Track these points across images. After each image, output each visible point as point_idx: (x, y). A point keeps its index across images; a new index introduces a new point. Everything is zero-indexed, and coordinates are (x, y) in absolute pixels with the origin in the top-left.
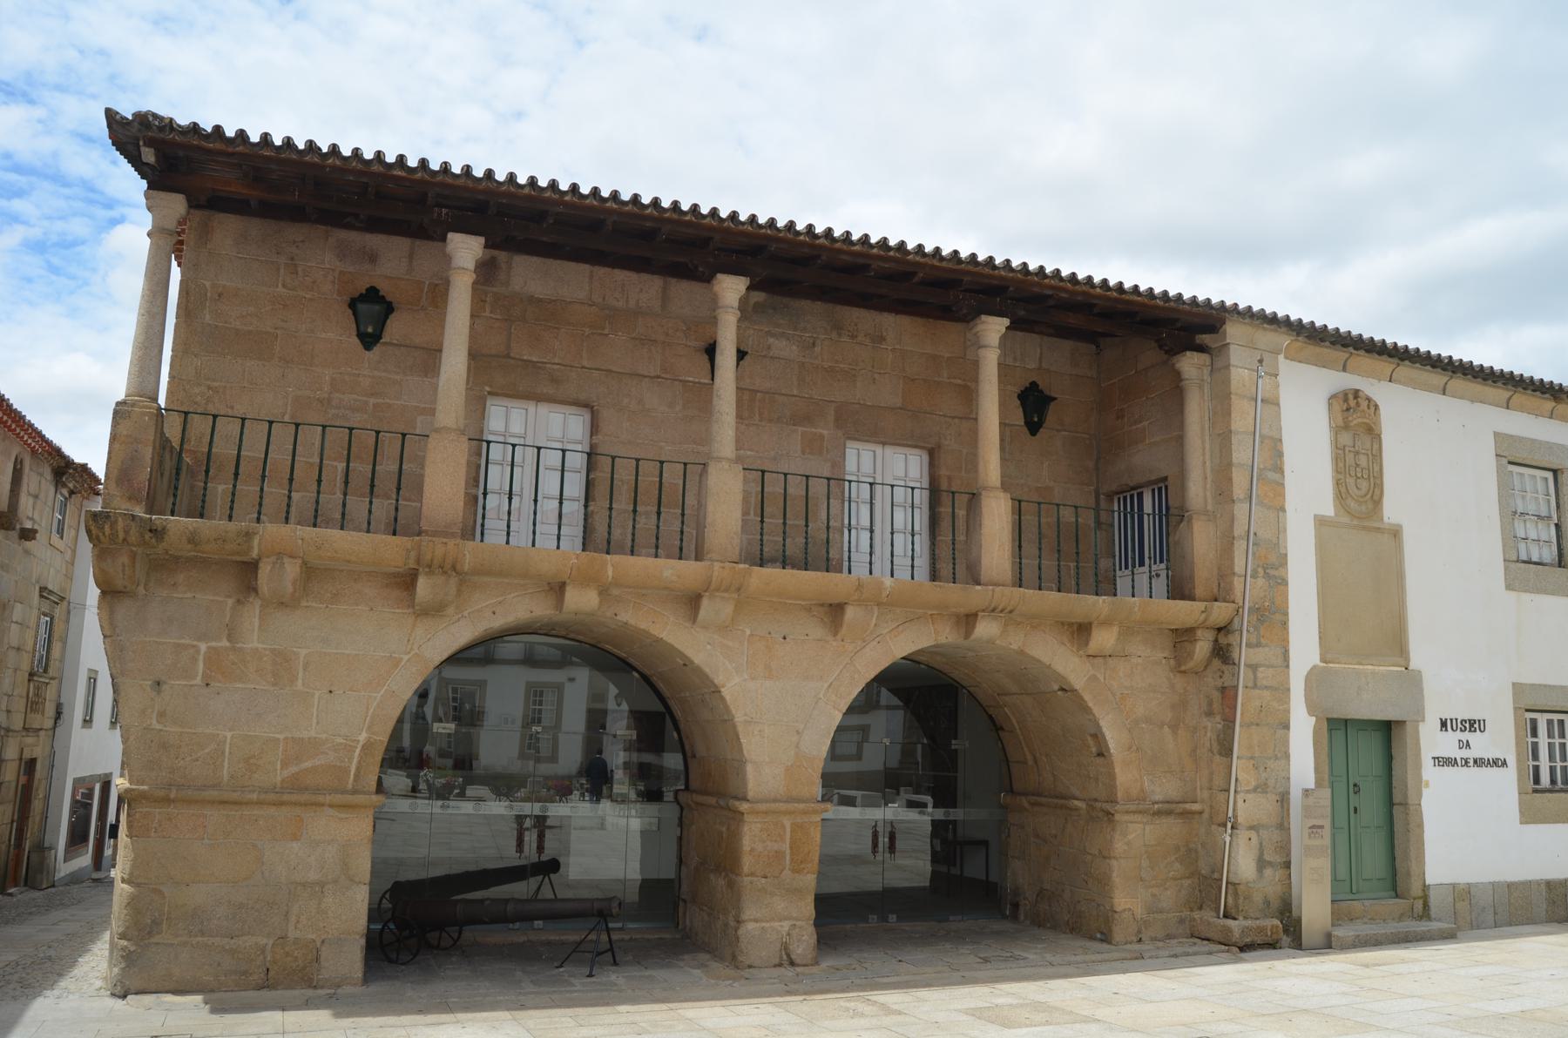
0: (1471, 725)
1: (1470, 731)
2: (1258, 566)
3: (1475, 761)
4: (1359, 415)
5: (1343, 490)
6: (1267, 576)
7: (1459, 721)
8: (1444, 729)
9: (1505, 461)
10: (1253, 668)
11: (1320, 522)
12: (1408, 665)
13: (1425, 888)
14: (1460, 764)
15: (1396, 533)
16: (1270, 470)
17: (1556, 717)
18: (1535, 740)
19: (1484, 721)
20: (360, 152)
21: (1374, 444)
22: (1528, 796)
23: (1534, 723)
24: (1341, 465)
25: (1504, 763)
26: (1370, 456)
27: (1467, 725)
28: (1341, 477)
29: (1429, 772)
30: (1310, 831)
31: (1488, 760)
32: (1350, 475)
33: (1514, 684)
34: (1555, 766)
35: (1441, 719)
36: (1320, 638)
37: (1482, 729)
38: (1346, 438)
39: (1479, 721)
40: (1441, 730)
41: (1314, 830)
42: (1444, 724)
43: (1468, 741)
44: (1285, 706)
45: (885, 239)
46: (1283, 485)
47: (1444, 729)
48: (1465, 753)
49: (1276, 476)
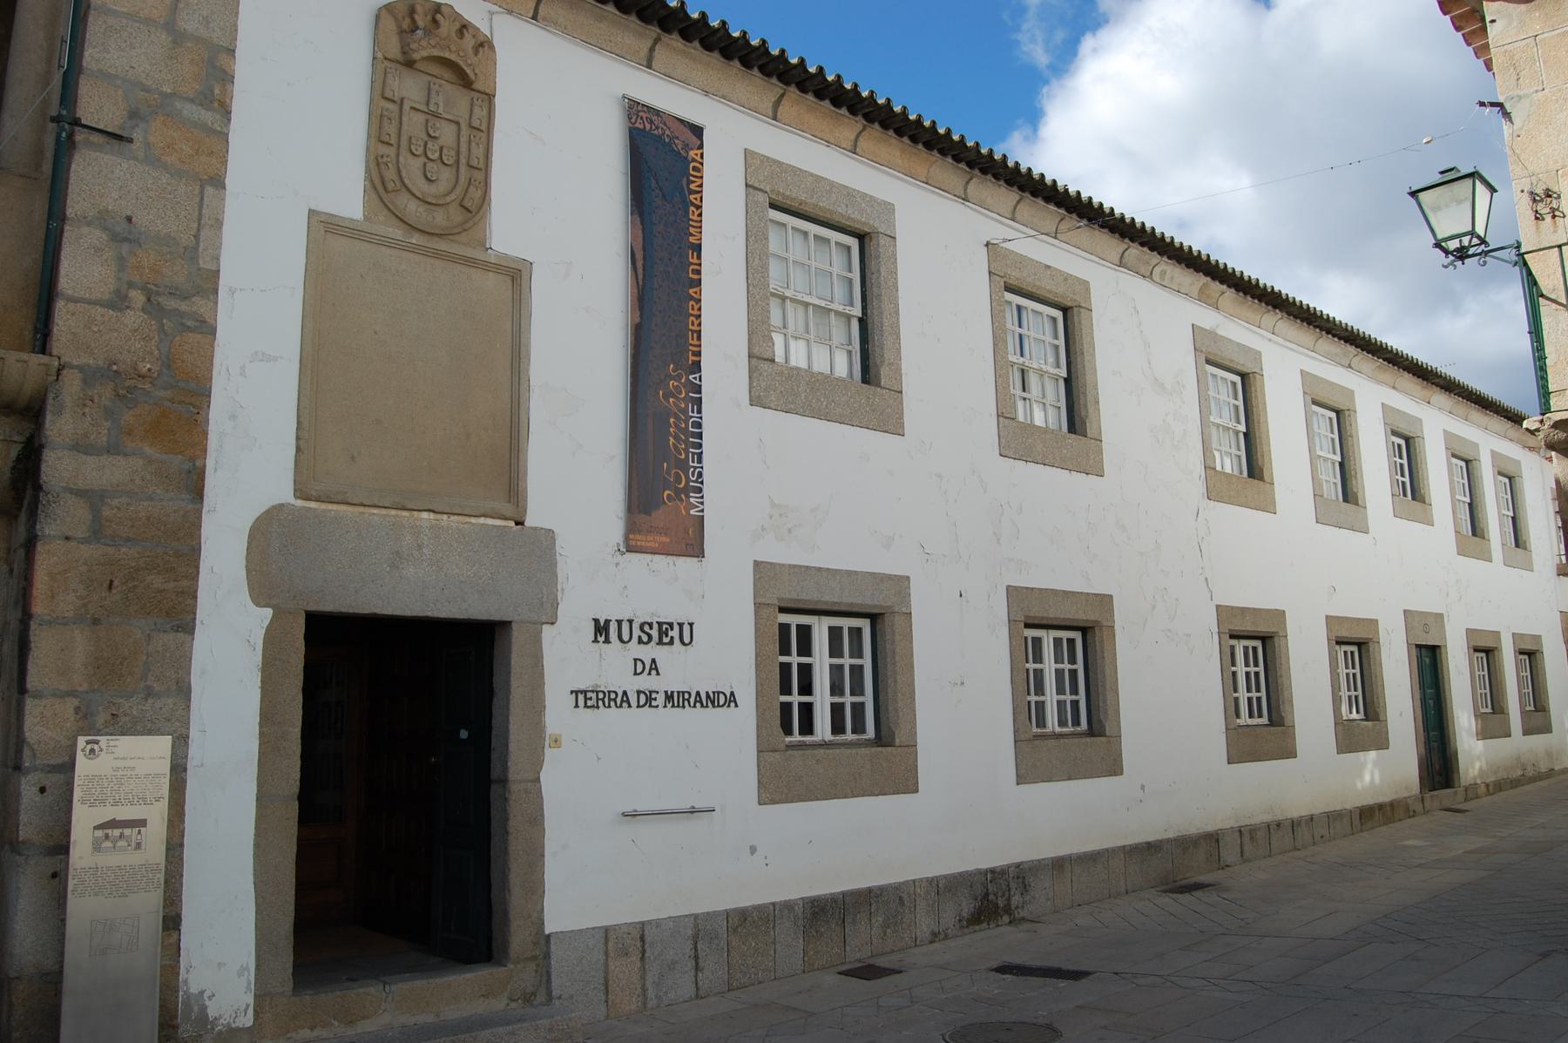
0: (663, 633)
1: (660, 642)
2: (131, 285)
3: (669, 697)
4: (433, 42)
5: (390, 174)
6: (152, 306)
7: (636, 626)
8: (601, 639)
9: (763, 199)
10: (94, 498)
11: (324, 227)
13: (545, 940)
14: (634, 702)
15: (516, 275)
16: (192, 101)
17: (846, 623)
18: (836, 661)
19: (691, 625)
21: (477, 110)
22: (777, 755)
23: (1037, 642)
24: (392, 129)
25: (732, 700)
26: (465, 131)
27: (655, 633)
28: (385, 150)
29: (558, 713)
30: (99, 833)
31: (698, 694)
32: (478, 159)
33: (757, 564)
34: (843, 705)
35: (596, 621)
36: (298, 449)
37: (687, 640)
38: (410, 87)
39: (681, 625)
40: (596, 641)
41: (117, 832)
42: (601, 629)
43: (653, 661)
44: (185, 583)
46: (224, 137)
47: (601, 639)
48: (647, 682)
49: (208, 117)
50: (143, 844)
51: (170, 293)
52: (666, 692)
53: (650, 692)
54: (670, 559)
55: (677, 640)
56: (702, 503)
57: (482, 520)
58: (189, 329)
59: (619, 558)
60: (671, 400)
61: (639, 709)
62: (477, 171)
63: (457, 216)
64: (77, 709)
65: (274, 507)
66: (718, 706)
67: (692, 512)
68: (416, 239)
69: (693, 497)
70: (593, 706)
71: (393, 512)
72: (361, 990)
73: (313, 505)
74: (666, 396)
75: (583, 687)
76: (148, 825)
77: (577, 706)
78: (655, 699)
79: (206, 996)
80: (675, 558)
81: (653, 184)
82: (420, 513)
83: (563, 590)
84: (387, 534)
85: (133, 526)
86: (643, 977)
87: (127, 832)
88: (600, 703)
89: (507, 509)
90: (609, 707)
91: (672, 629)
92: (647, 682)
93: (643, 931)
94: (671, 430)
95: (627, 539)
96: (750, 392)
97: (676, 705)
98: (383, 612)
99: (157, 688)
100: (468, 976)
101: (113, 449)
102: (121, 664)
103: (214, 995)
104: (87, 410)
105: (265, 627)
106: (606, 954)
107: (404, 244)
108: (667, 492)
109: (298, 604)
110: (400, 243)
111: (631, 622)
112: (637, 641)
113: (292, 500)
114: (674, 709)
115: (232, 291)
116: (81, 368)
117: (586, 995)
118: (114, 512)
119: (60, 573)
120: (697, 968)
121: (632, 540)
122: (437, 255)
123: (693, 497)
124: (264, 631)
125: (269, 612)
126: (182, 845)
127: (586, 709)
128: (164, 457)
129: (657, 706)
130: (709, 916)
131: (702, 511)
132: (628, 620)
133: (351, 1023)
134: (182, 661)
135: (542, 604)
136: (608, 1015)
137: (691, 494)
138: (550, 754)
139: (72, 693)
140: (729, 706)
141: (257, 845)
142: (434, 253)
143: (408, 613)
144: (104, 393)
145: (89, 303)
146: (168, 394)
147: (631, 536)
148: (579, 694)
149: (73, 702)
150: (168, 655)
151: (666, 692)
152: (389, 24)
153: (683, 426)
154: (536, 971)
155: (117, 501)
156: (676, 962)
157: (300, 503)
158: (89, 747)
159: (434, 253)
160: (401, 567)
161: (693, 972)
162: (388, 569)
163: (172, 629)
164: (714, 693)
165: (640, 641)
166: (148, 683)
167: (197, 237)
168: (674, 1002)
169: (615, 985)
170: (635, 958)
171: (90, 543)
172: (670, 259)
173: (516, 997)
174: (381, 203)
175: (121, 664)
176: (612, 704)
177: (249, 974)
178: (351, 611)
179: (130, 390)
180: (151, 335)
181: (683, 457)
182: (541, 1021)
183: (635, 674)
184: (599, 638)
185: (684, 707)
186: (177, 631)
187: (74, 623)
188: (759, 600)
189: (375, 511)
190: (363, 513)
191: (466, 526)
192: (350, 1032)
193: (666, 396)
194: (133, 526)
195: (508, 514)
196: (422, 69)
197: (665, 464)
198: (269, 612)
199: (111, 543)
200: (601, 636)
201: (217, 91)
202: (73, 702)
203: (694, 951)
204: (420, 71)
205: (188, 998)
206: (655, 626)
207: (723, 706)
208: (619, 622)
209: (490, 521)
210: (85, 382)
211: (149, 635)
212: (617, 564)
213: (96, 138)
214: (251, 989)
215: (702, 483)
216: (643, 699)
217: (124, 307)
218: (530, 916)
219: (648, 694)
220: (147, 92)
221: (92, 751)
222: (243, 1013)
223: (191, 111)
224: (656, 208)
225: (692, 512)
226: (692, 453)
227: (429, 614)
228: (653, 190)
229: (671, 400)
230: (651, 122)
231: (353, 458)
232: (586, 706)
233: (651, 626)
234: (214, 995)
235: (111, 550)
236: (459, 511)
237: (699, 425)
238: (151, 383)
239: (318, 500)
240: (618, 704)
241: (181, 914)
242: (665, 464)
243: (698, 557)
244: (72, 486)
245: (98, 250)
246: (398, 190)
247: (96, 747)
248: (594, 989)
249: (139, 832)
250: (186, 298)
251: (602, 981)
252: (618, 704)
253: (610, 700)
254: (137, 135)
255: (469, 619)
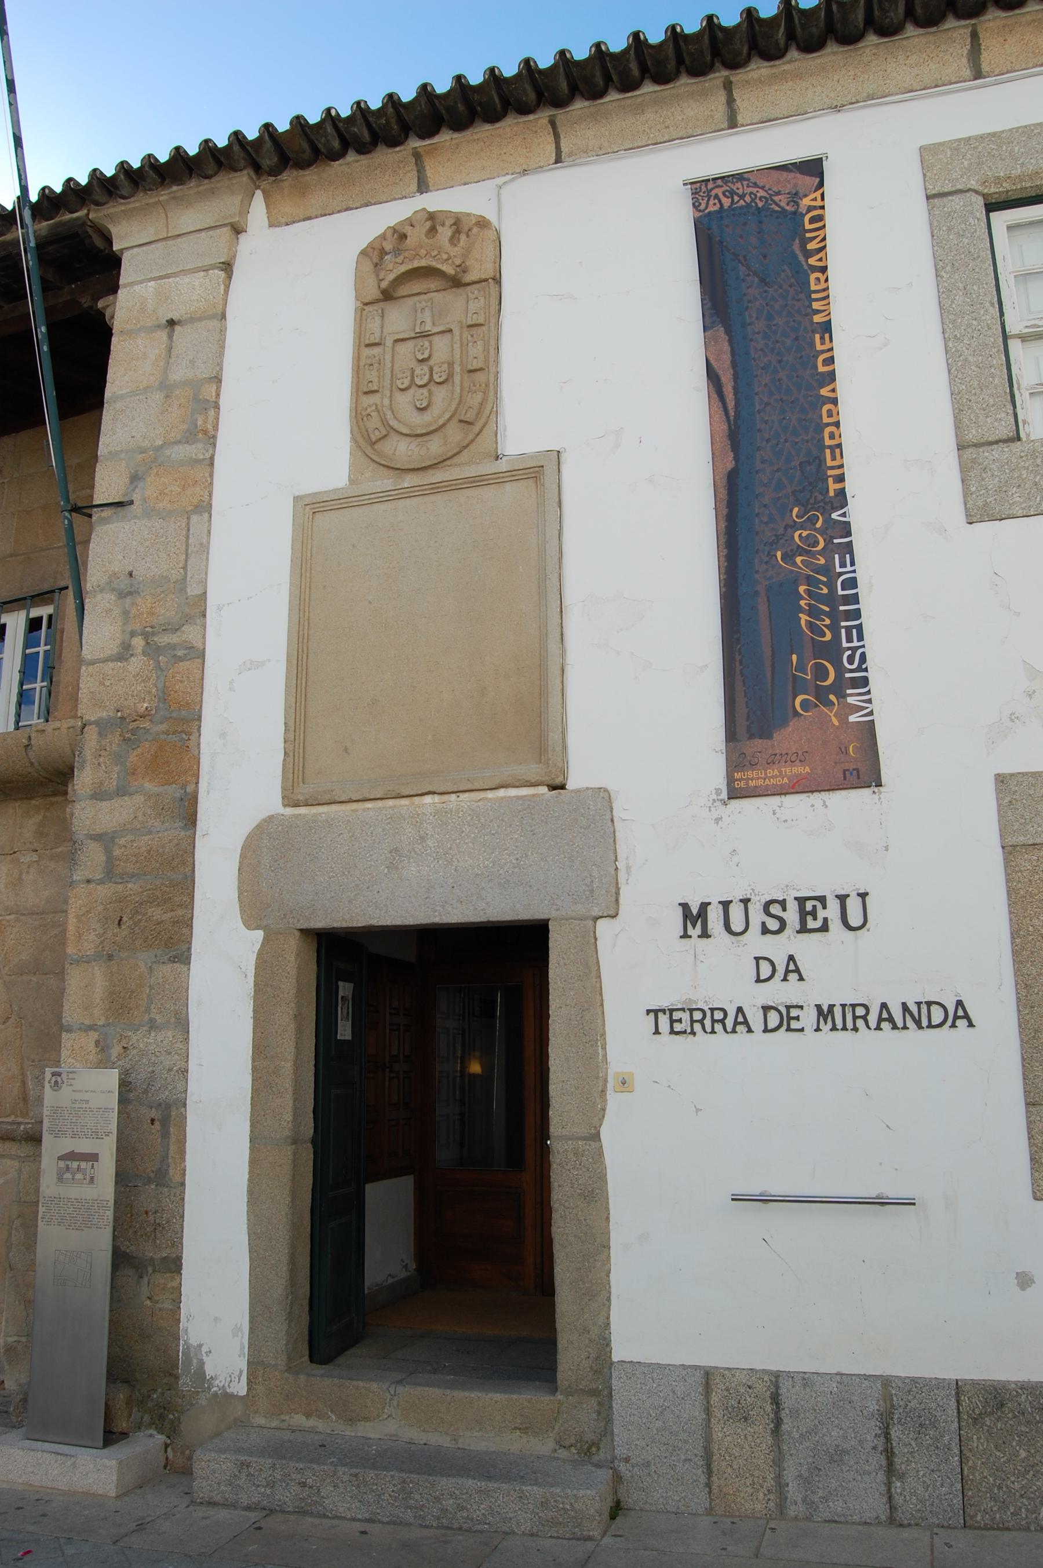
1: (803, 929)
2: (133, 634)
3: (824, 1014)
6: (152, 650)
8: (695, 932)
10: (106, 840)
12: (564, 772)
16: (179, 442)
20: (395, 98)
27: (792, 916)
30: (62, 1164)
35: (685, 907)
37: (855, 920)
40: (685, 936)
41: (75, 1165)
44: (180, 912)
45: (178, 149)
48: (779, 993)
50: (95, 1179)
51: (164, 630)
52: (819, 1007)
53: (788, 1008)
54: (816, 798)
55: (835, 924)
56: (869, 701)
57: (502, 793)
58: (181, 659)
59: (721, 811)
60: (798, 560)
61: (768, 1034)
62: (478, 373)
63: (454, 434)
64: (97, 1043)
65: (265, 820)
66: (930, 1026)
67: (853, 718)
68: (409, 481)
69: (851, 695)
70: (685, 1032)
71: (390, 803)
72: (361, 1384)
73: (303, 810)
74: (788, 557)
75: (665, 1004)
76: (100, 1160)
77: (657, 1032)
78: (797, 1018)
79: (204, 1349)
80: (824, 795)
81: (742, 271)
82: (423, 797)
83: (628, 868)
84: (384, 830)
85: (137, 862)
86: (778, 1462)
87: (83, 1165)
88: (697, 1027)
89: (532, 770)
90: (713, 1032)
91: (824, 907)
92: (779, 993)
93: (777, 1387)
94: (802, 603)
95: (730, 780)
96: (966, 504)
97: (839, 1025)
98: (380, 924)
99: (159, 1021)
100: (498, 1396)
101: (122, 792)
102: (130, 997)
103: (210, 1352)
104: (101, 760)
105: (257, 951)
106: (708, 1410)
107: (396, 492)
108: (799, 699)
109: (289, 922)
110: (392, 493)
111: (746, 902)
112: (759, 928)
113: (282, 810)
114: (834, 1032)
115: (220, 608)
116: (97, 723)
117: (673, 1467)
118: (122, 850)
119: (84, 915)
120: (890, 1470)
121: (740, 780)
122: (436, 489)
123: (851, 695)
124: (255, 955)
125: (259, 934)
126: (183, 1184)
127: (674, 1036)
128: (161, 789)
129: (802, 1030)
130: (915, 1384)
131: (871, 713)
132: (741, 901)
133: (351, 1421)
134: (181, 994)
135: (592, 891)
136: (712, 1509)
137: (849, 691)
138: (614, 1101)
139: (92, 1028)
140: (953, 1026)
141: (250, 1192)
142: (432, 489)
143: (410, 921)
144: (114, 740)
145: (103, 662)
146: (162, 727)
147: (737, 776)
148: (660, 1015)
149: (94, 1036)
150: (167, 986)
151: (819, 1007)
152: (368, 266)
153: (825, 591)
154: (599, 1413)
155: (123, 839)
156: (846, 1452)
157: (289, 811)
158: (54, 1079)
159: (432, 489)
160: (400, 867)
161: (881, 1477)
162: (386, 870)
163: (170, 960)
164: (919, 1004)
165: (765, 930)
166: (152, 1016)
167: (185, 568)
168: (842, 1519)
169: (724, 1464)
170: (762, 1428)
171: (104, 883)
172: (780, 362)
173: (567, 1443)
174: (367, 459)
175: (130, 997)
176: (860, 1023)
177: (243, 1335)
178: (344, 925)
179: (134, 732)
180: (150, 675)
181: (828, 636)
182: (529, 1488)
183: (758, 980)
184: (690, 931)
185: (855, 1029)
186: (174, 962)
187: (95, 961)
188: (1011, 840)
189: (369, 805)
190: (355, 810)
191: (479, 804)
192: (349, 1432)
193: (788, 557)
194: (137, 862)
195: (535, 778)
196: (405, 294)
197: (794, 657)
198: (259, 934)
199: (120, 881)
200: (694, 927)
201: (200, 422)
202: (94, 1036)
203: (882, 1439)
204: (404, 297)
205: (188, 1348)
206: (793, 907)
207: (940, 1025)
208: (726, 905)
209: (513, 792)
210: (100, 734)
211: (150, 967)
212: (718, 820)
213: (107, 512)
214: (244, 1354)
215: (866, 670)
216: (773, 1019)
217: (129, 655)
218: (586, 1330)
219: (784, 1011)
220: (143, 453)
221: (56, 1082)
222: (237, 1378)
223: (181, 451)
224: (749, 302)
225: (853, 718)
226: (847, 628)
227: (437, 920)
228: (743, 280)
229: (798, 560)
230: (732, 193)
231: (346, 750)
232: (672, 1032)
233: (783, 904)
234: (210, 1352)
235: (120, 887)
236: (469, 787)
237: (852, 583)
238: (150, 720)
239: (307, 805)
240: (729, 1028)
241: (182, 1257)
242: (794, 657)
243: (870, 787)
244: (92, 832)
245: (109, 611)
246: (386, 436)
247: (59, 1079)
248: (685, 1460)
249: (93, 1167)
250: (176, 630)
251: (700, 1452)
252: (729, 1028)
253: (714, 1021)
254: (136, 497)
255: (488, 922)
